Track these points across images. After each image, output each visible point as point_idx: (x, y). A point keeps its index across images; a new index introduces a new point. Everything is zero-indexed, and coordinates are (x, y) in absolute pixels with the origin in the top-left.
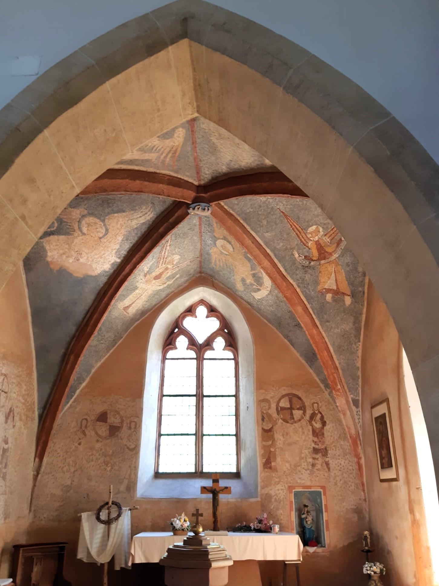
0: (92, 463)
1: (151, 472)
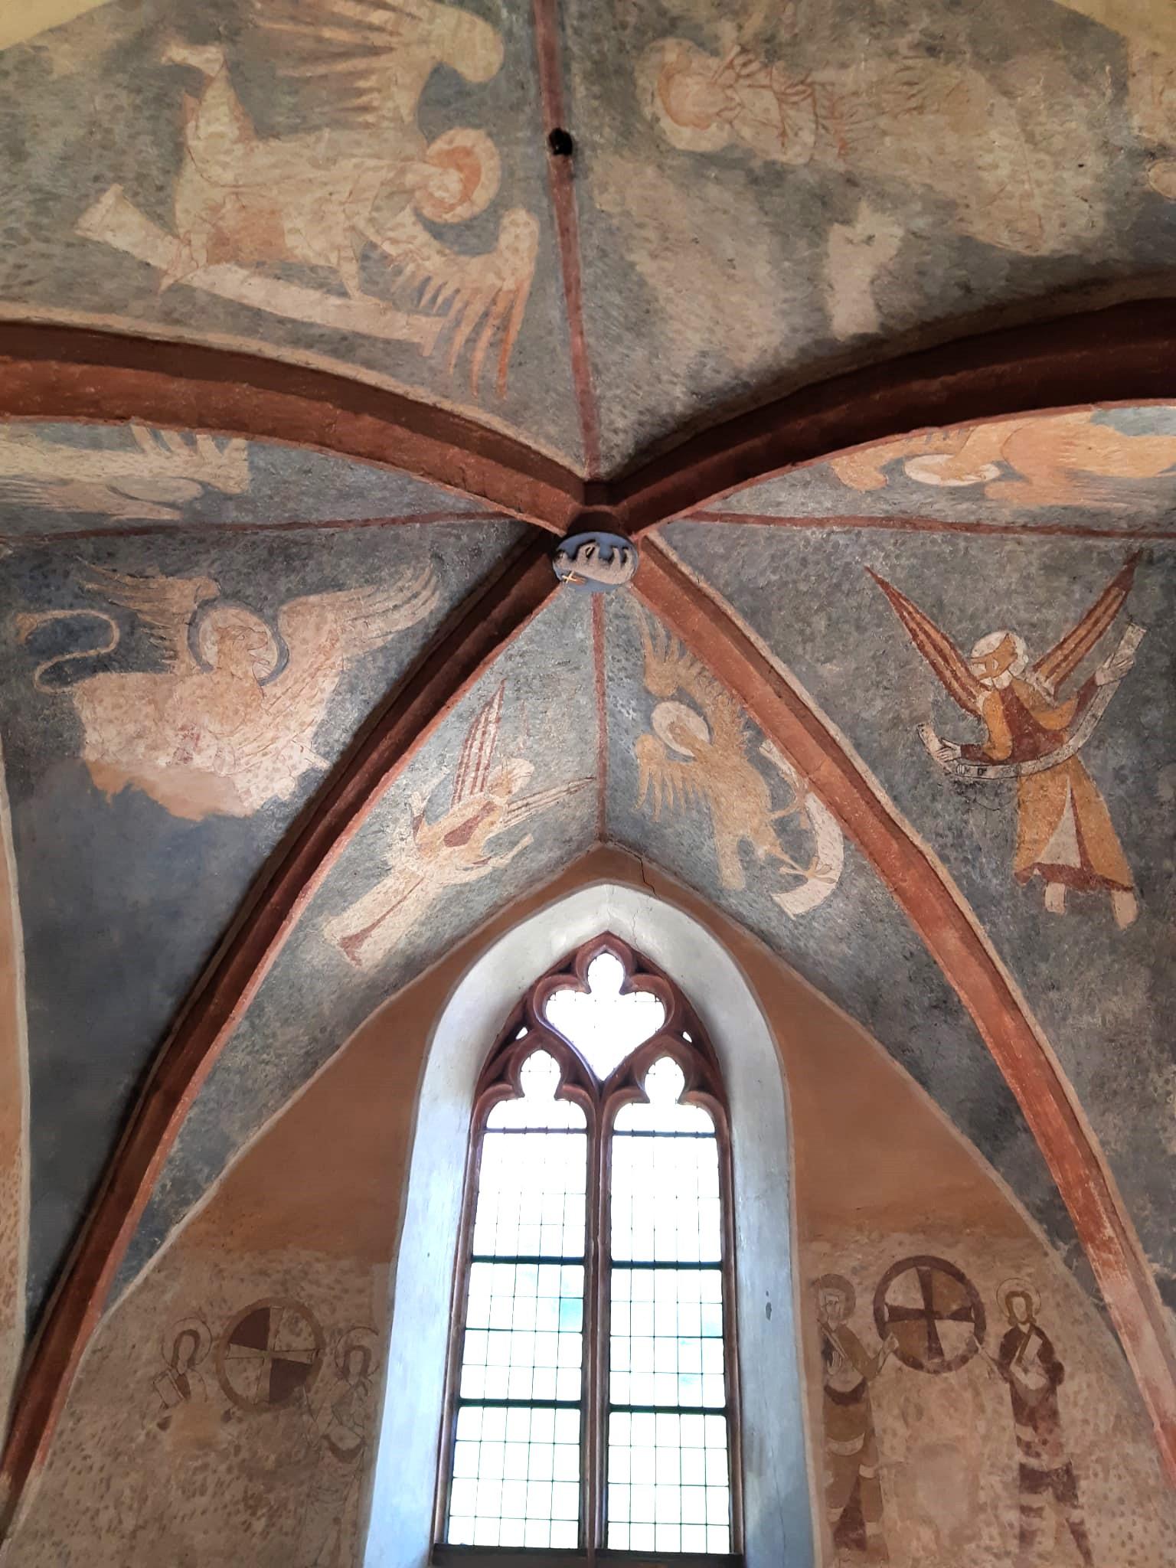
0: (201, 1501)
1: (419, 1544)
